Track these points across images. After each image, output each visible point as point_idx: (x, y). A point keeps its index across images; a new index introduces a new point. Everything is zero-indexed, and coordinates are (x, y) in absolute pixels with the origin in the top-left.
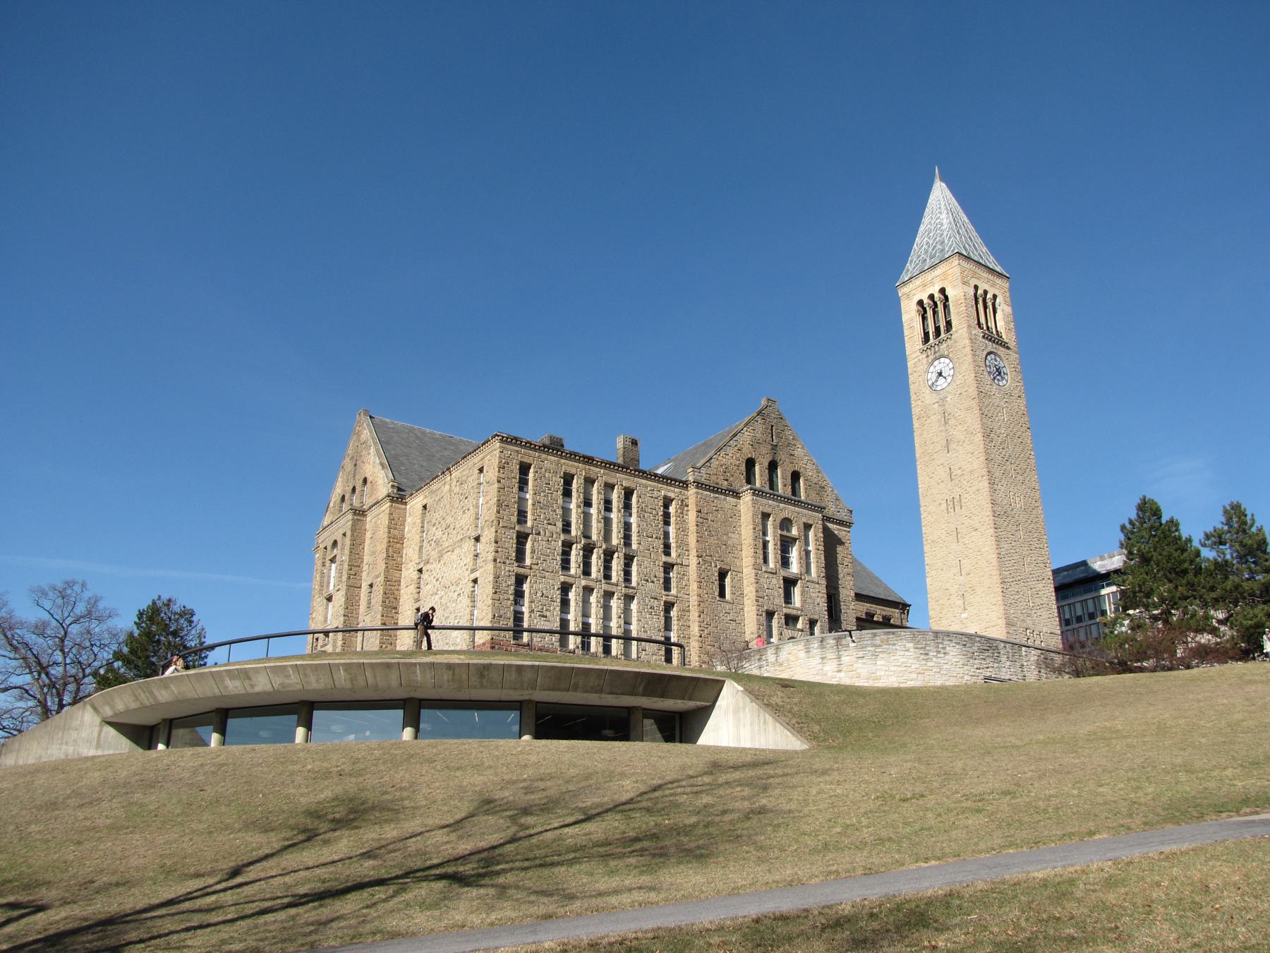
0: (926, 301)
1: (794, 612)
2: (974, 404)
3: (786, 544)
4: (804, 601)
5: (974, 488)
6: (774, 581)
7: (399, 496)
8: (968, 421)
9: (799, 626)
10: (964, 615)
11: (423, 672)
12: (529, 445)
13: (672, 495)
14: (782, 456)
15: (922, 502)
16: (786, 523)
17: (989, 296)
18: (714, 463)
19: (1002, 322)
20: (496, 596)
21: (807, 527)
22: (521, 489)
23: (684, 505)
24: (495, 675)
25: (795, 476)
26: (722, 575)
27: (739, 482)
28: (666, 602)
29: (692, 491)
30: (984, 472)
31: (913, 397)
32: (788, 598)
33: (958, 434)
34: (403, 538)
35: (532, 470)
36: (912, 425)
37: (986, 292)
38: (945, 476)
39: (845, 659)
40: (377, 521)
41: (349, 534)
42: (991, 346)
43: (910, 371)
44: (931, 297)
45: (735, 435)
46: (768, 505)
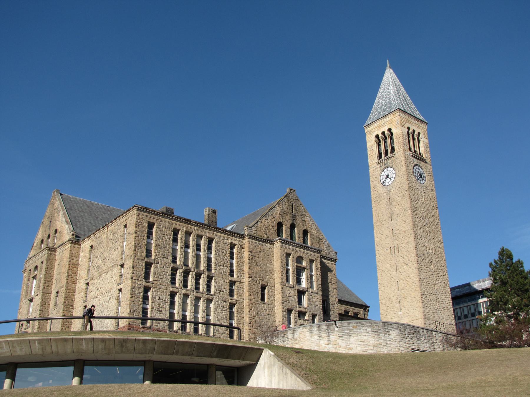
0: (380, 135)
2: (407, 193)
3: (299, 271)
4: (309, 304)
5: (406, 241)
6: (292, 292)
7: (76, 240)
8: (403, 203)
9: (306, 318)
10: (400, 313)
11: (87, 344)
12: (154, 212)
13: (235, 242)
14: (298, 221)
17: (416, 133)
18: (260, 224)
19: (423, 148)
20: (132, 299)
21: (312, 261)
23: (242, 248)
24: (130, 346)
25: (305, 233)
26: (263, 288)
27: (273, 236)
28: (230, 303)
29: (247, 240)
31: (372, 189)
32: (300, 302)
33: (397, 210)
34: (78, 264)
35: (155, 227)
36: (371, 205)
37: (414, 131)
38: (390, 234)
39: (332, 337)
40: (63, 255)
41: (45, 262)
42: (416, 161)
43: (370, 174)
44: (383, 133)
45: (271, 209)
46: (289, 248)
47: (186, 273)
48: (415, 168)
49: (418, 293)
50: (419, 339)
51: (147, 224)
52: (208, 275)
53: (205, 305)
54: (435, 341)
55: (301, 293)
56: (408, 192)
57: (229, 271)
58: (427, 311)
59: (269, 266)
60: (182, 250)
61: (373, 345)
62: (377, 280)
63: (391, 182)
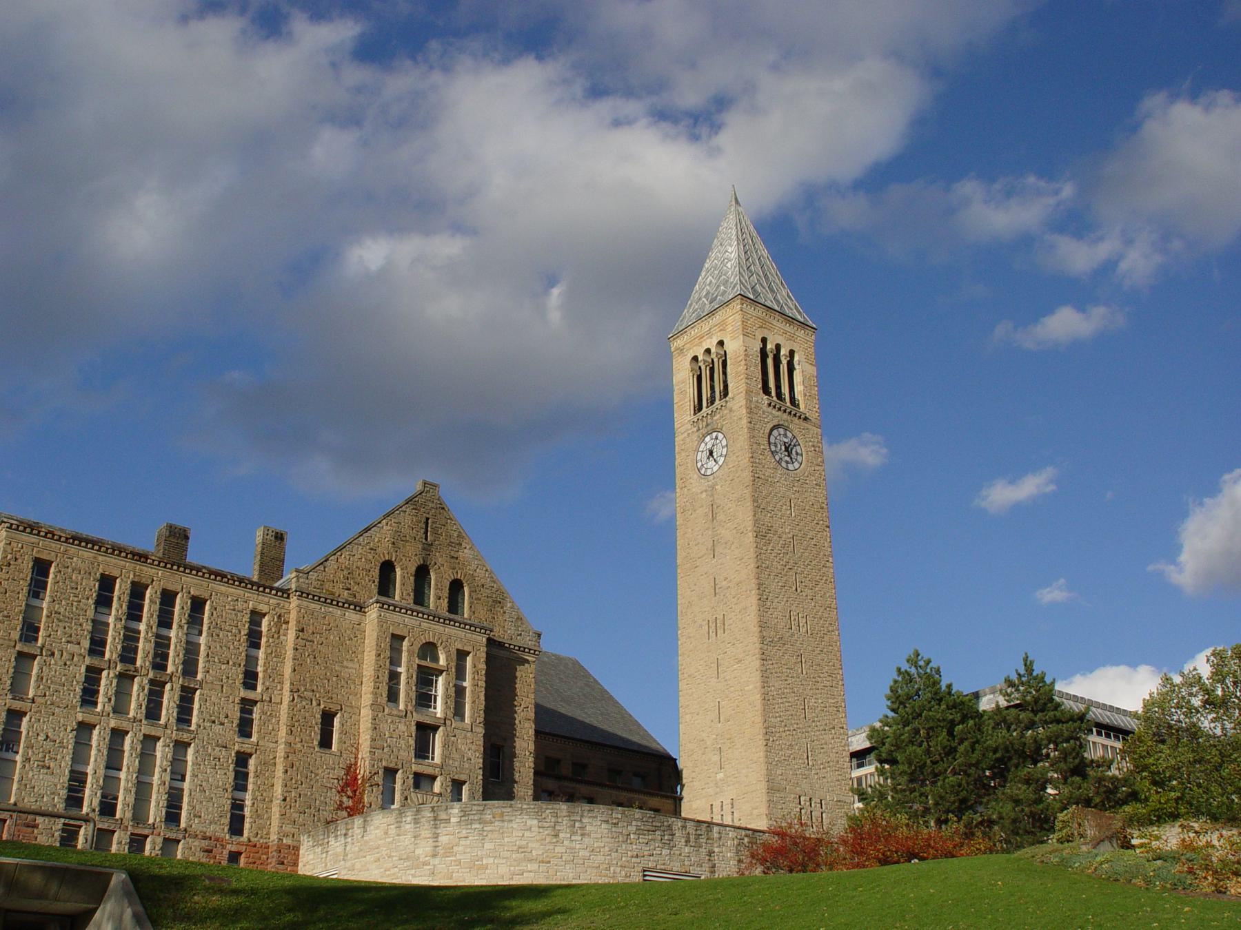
1: (429, 771)
2: (747, 493)
3: (425, 678)
4: (445, 757)
6: (402, 727)
8: (740, 514)
9: (437, 787)
10: (720, 776)
12: (50, 535)
13: (263, 608)
15: (681, 622)
16: (429, 649)
18: (331, 564)
22: (36, 595)
23: (281, 620)
25: (456, 587)
28: (238, 753)
29: (294, 601)
30: (753, 584)
32: (423, 750)
35: (52, 570)
37: (778, 347)
39: (443, 839)
45: (367, 530)
47: (125, 678)
48: (775, 432)
49: (759, 729)
50: (670, 845)
51: (31, 565)
52: (182, 687)
53: (170, 756)
54: (716, 850)
55: (425, 731)
56: (750, 489)
57: (241, 676)
58: (779, 772)
59: (350, 665)
60: (119, 626)
61: (540, 859)
62: (678, 696)
63: (715, 469)
